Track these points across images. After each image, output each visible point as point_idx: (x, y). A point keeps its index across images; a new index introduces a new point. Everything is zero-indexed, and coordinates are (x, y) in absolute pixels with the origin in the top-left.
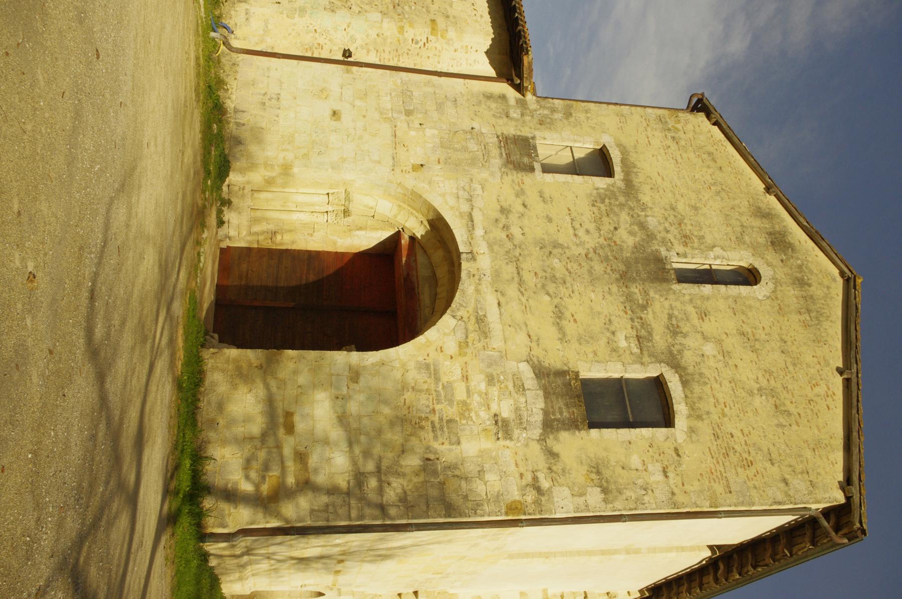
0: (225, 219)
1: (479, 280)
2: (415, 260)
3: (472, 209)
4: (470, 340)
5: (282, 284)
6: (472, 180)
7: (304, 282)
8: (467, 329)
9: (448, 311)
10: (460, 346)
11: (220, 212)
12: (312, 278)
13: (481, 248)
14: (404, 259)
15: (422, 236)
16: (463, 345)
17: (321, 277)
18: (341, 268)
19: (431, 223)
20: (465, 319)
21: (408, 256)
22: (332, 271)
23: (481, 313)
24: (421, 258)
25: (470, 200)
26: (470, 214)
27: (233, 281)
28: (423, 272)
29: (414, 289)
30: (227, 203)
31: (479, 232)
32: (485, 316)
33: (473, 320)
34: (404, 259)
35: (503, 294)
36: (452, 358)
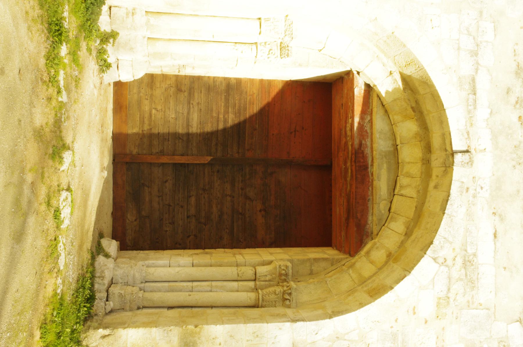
0: (111, 60)
1: (474, 196)
2: (371, 121)
3: (477, 70)
4: (452, 295)
5: (194, 129)
6: (481, 13)
7: (221, 126)
8: (449, 278)
9: (429, 252)
10: (438, 305)
11: (101, 52)
12: (232, 120)
13: (482, 140)
14: (357, 120)
15: (387, 92)
16: (444, 302)
17: (242, 119)
18: (268, 105)
19: (406, 80)
20: (449, 262)
21: (362, 118)
22: (255, 109)
23: (470, 251)
24: (379, 124)
25: (474, 54)
26: (473, 80)
27: (133, 129)
28: (380, 144)
29: (366, 168)
30: (108, 37)
31: (482, 113)
32: (475, 255)
33: (459, 261)
34: (357, 120)
35: (502, 219)
36: (426, 322)
